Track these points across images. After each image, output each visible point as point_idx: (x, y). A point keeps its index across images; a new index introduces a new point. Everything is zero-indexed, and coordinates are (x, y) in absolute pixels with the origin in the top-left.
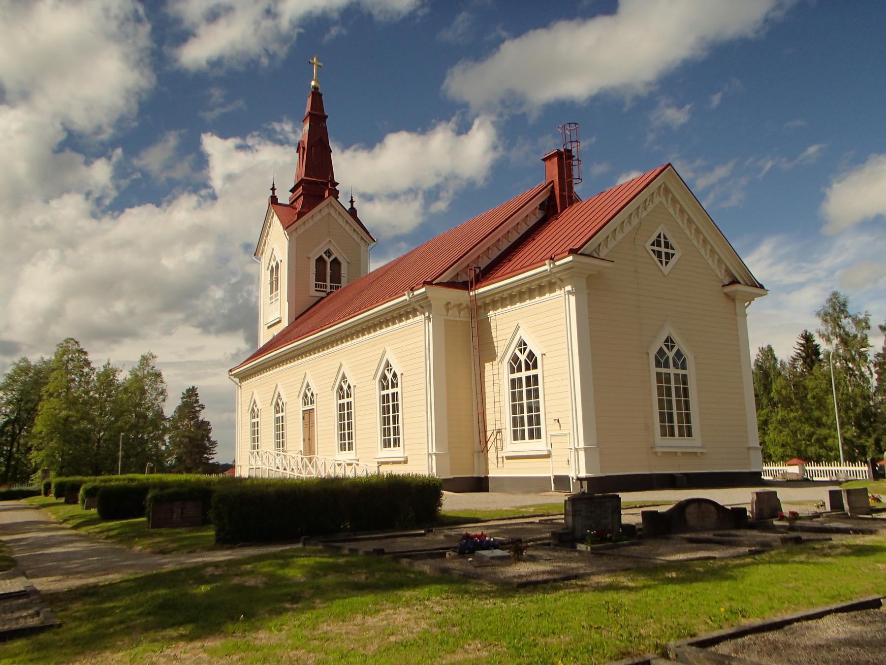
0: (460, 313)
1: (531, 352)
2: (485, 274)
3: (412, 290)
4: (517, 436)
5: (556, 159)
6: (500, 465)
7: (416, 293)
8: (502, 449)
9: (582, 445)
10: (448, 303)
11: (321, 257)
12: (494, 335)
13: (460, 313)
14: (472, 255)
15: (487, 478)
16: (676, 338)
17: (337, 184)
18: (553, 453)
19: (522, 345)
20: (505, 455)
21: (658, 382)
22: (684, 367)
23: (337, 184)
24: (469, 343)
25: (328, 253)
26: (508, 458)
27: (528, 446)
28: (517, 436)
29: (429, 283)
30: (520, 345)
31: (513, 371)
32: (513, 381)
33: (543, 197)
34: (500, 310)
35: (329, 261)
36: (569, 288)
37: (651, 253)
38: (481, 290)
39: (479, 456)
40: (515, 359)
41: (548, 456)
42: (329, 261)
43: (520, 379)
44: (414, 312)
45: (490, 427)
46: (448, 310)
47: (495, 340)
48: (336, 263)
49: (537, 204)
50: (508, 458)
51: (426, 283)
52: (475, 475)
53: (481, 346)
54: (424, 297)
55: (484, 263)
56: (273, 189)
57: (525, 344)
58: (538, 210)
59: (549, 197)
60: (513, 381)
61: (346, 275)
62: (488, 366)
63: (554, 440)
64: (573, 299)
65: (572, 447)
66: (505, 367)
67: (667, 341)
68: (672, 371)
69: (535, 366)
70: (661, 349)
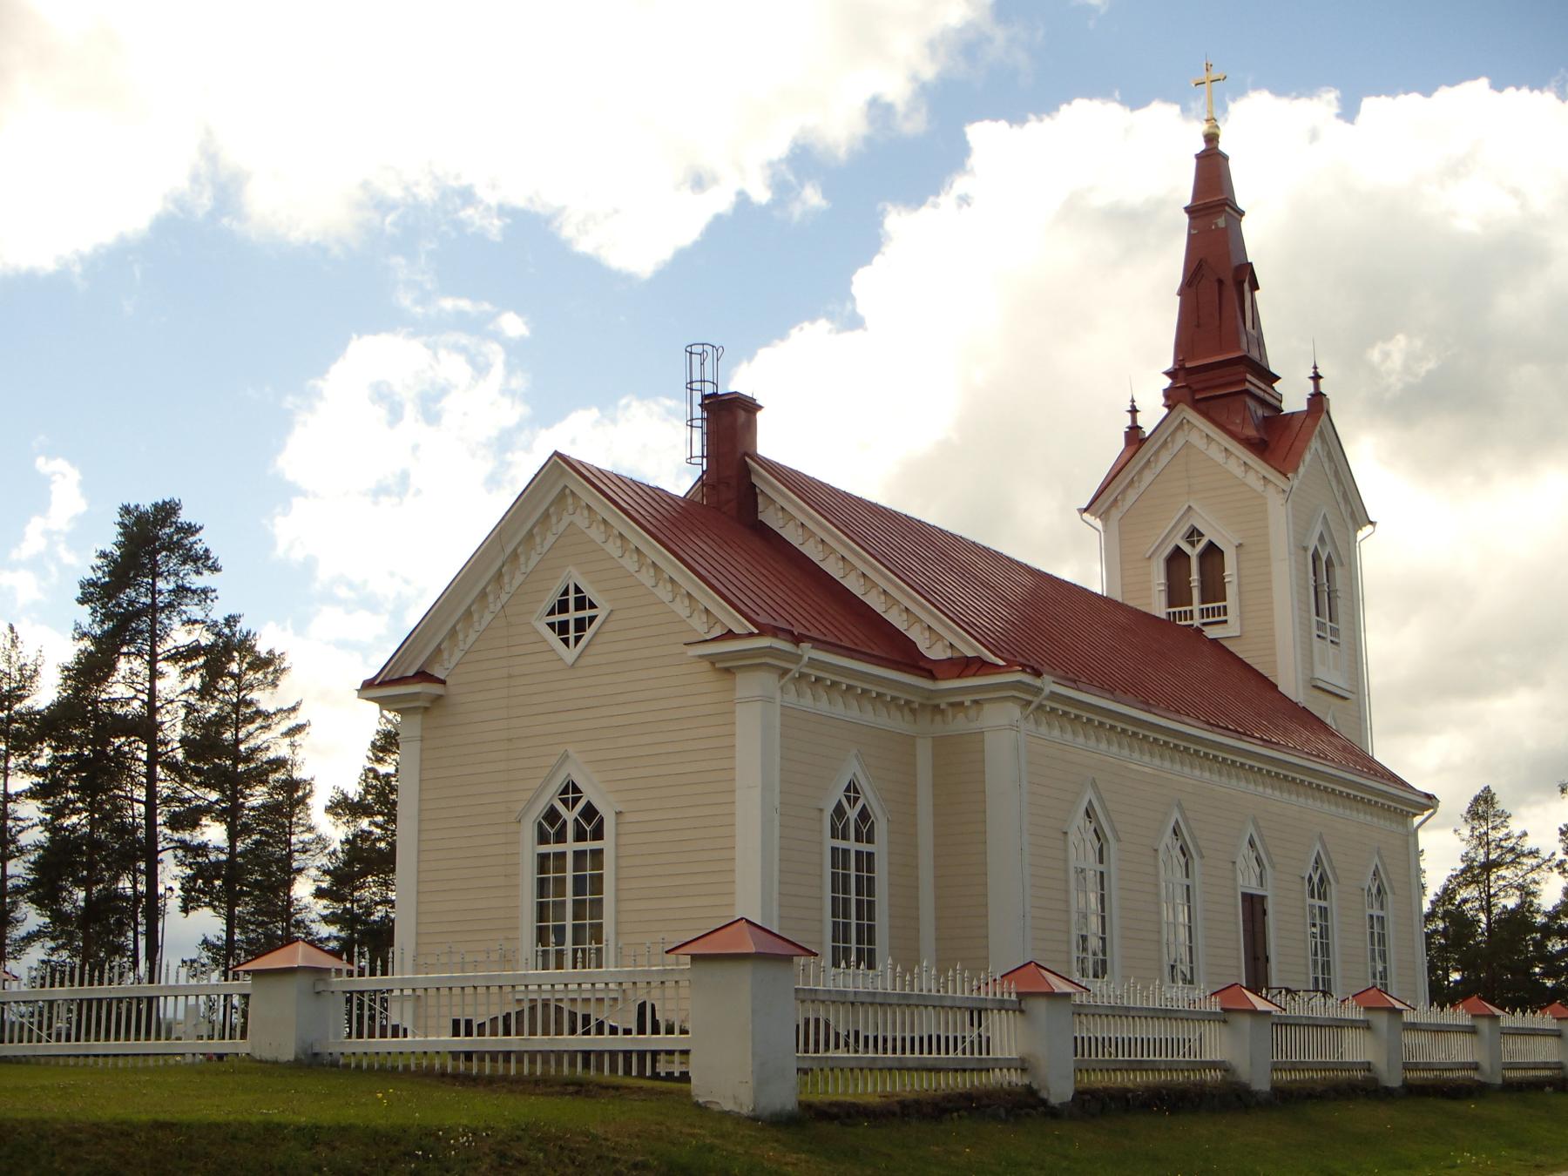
1: (589, 806)
11: (1178, 548)
16: (863, 784)
17: (1277, 378)
19: (571, 792)
21: (601, 876)
22: (870, 840)
23: (1277, 378)
25: (1193, 535)
30: (565, 791)
31: (543, 838)
32: (543, 858)
35: (1193, 553)
37: (582, 643)
40: (552, 815)
42: (1193, 553)
43: (561, 856)
48: (1212, 553)
56: (1316, 378)
57: (576, 790)
60: (543, 858)
61: (1234, 579)
67: (848, 789)
68: (852, 845)
69: (598, 834)
70: (840, 804)
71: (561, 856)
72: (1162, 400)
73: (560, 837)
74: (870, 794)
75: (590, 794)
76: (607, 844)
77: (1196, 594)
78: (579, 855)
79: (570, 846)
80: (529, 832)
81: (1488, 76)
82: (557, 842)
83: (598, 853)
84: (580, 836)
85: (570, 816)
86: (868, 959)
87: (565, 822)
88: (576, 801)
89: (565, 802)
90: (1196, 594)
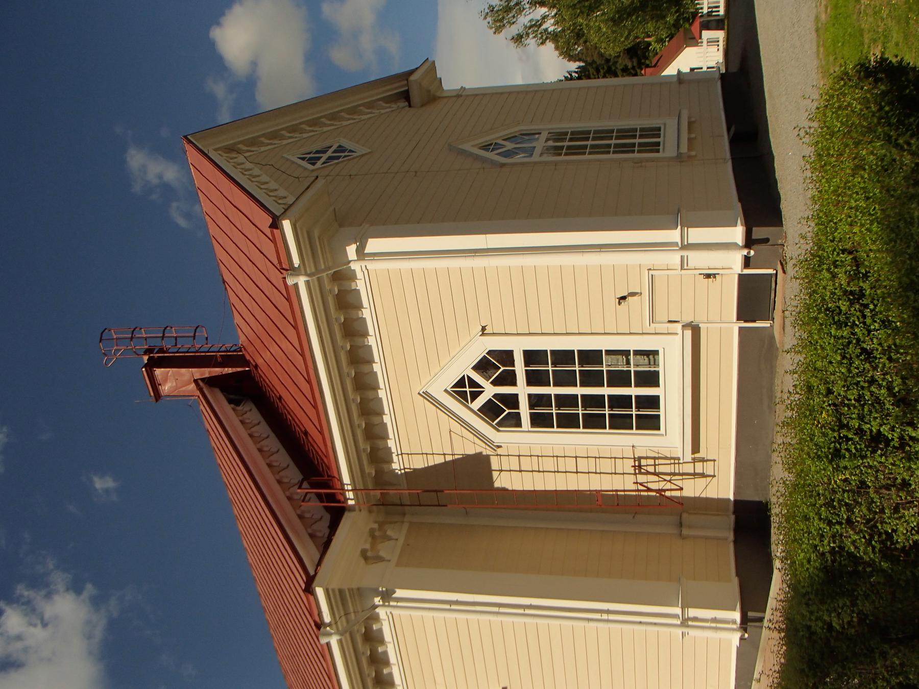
0: (389, 539)
2: (313, 468)
3: (319, 625)
4: (651, 423)
5: (158, 372)
6: (709, 469)
7: (327, 618)
8: (675, 460)
9: (677, 611)
10: (364, 554)
12: (439, 460)
13: (389, 539)
14: (277, 495)
15: (736, 502)
18: (687, 319)
19: (464, 389)
20: (689, 457)
24: (455, 518)
26: (696, 448)
27: (672, 393)
28: (651, 423)
29: (310, 581)
30: (463, 395)
31: (515, 421)
33: (219, 399)
34: (391, 443)
36: (351, 250)
38: (346, 479)
39: (690, 527)
40: (490, 411)
41: (696, 330)
43: (535, 401)
44: (373, 638)
45: (626, 484)
46: (379, 559)
47: (449, 458)
49: (228, 408)
50: (696, 448)
51: (309, 589)
52: (731, 537)
53: (463, 485)
54: (338, 598)
55: (293, 474)
57: (460, 383)
58: (239, 408)
59: (222, 391)
62: (501, 481)
63: (661, 315)
64: (374, 245)
65: (679, 631)
66: (506, 438)
69: (506, 357)
71: (535, 401)
72: (557, 53)
73: (512, 401)
74: (497, 135)
75: (464, 366)
76: (518, 346)
77: (616, 412)
78: (534, 379)
79: (522, 390)
80: (480, 348)
81: (208, 33)
82: (517, 406)
83: (531, 357)
84: (509, 379)
85: (489, 391)
86: (655, 132)
87: (495, 396)
88: (473, 384)
89: (475, 396)
90: (616, 412)
